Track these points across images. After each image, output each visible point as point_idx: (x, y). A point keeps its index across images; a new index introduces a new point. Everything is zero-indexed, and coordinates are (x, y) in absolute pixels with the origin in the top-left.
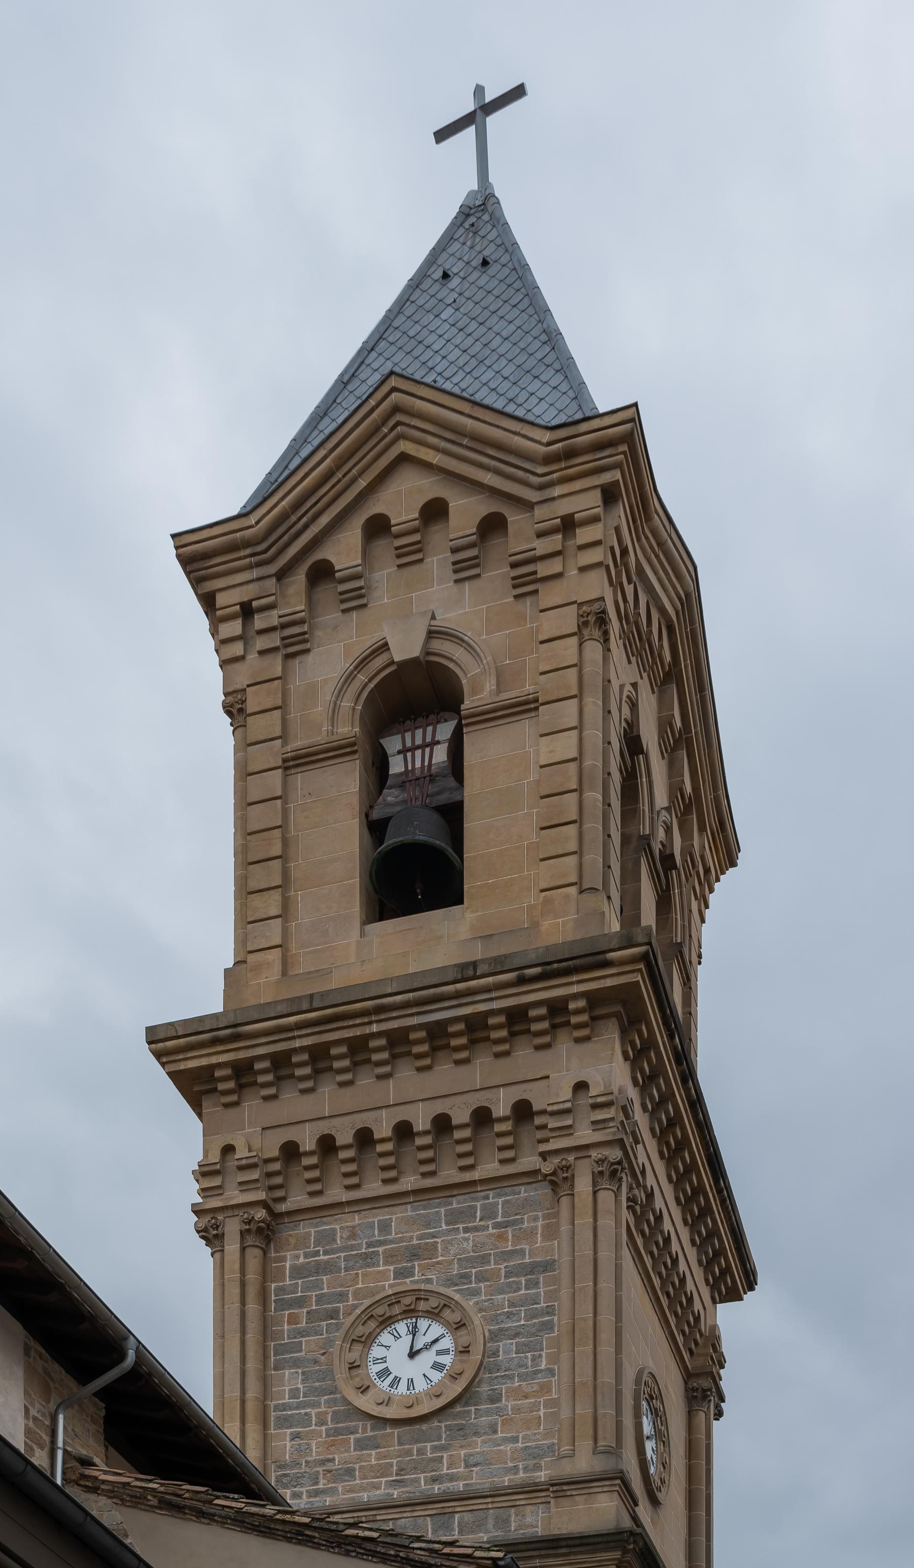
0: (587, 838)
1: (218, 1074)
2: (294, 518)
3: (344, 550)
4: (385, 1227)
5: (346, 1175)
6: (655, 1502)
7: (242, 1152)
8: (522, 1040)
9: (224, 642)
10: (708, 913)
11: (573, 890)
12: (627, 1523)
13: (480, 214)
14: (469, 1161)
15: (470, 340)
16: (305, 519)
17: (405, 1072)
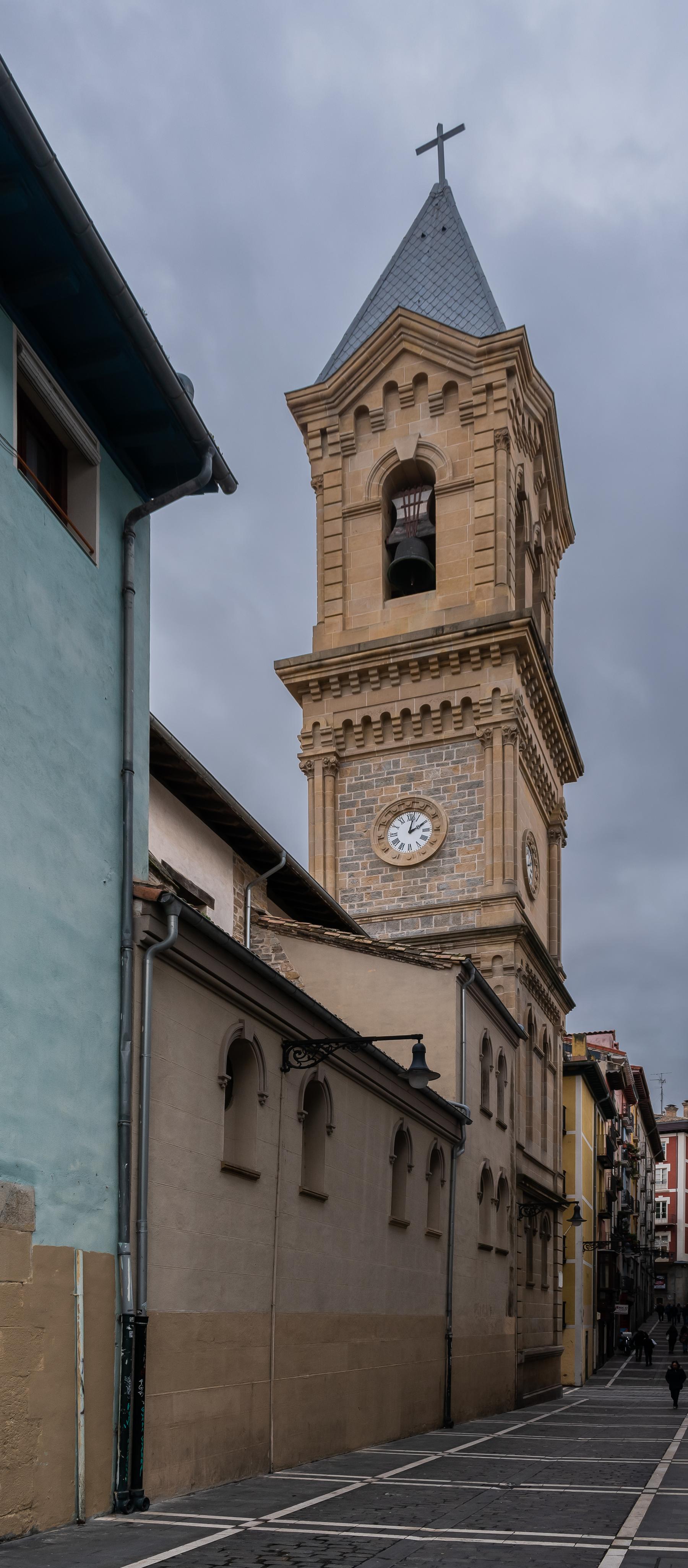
0: (499, 556)
1: (311, 685)
2: (348, 384)
3: (374, 401)
4: (396, 764)
5: (376, 737)
6: (532, 899)
7: (323, 726)
8: (466, 665)
9: (312, 449)
10: (559, 571)
11: (492, 585)
12: (520, 920)
13: (441, 196)
14: (440, 729)
15: (437, 277)
16: (353, 385)
17: (407, 682)
